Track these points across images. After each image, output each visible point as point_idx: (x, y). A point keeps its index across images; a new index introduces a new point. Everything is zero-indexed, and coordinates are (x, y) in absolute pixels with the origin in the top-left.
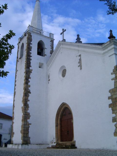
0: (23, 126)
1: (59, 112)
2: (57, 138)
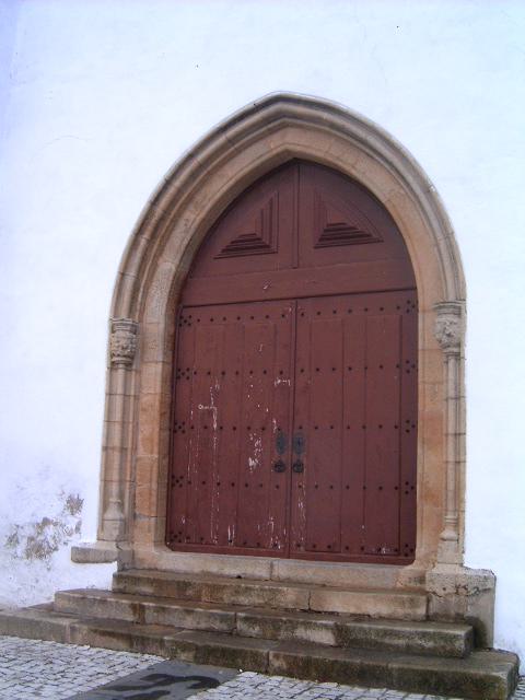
2: (121, 505)
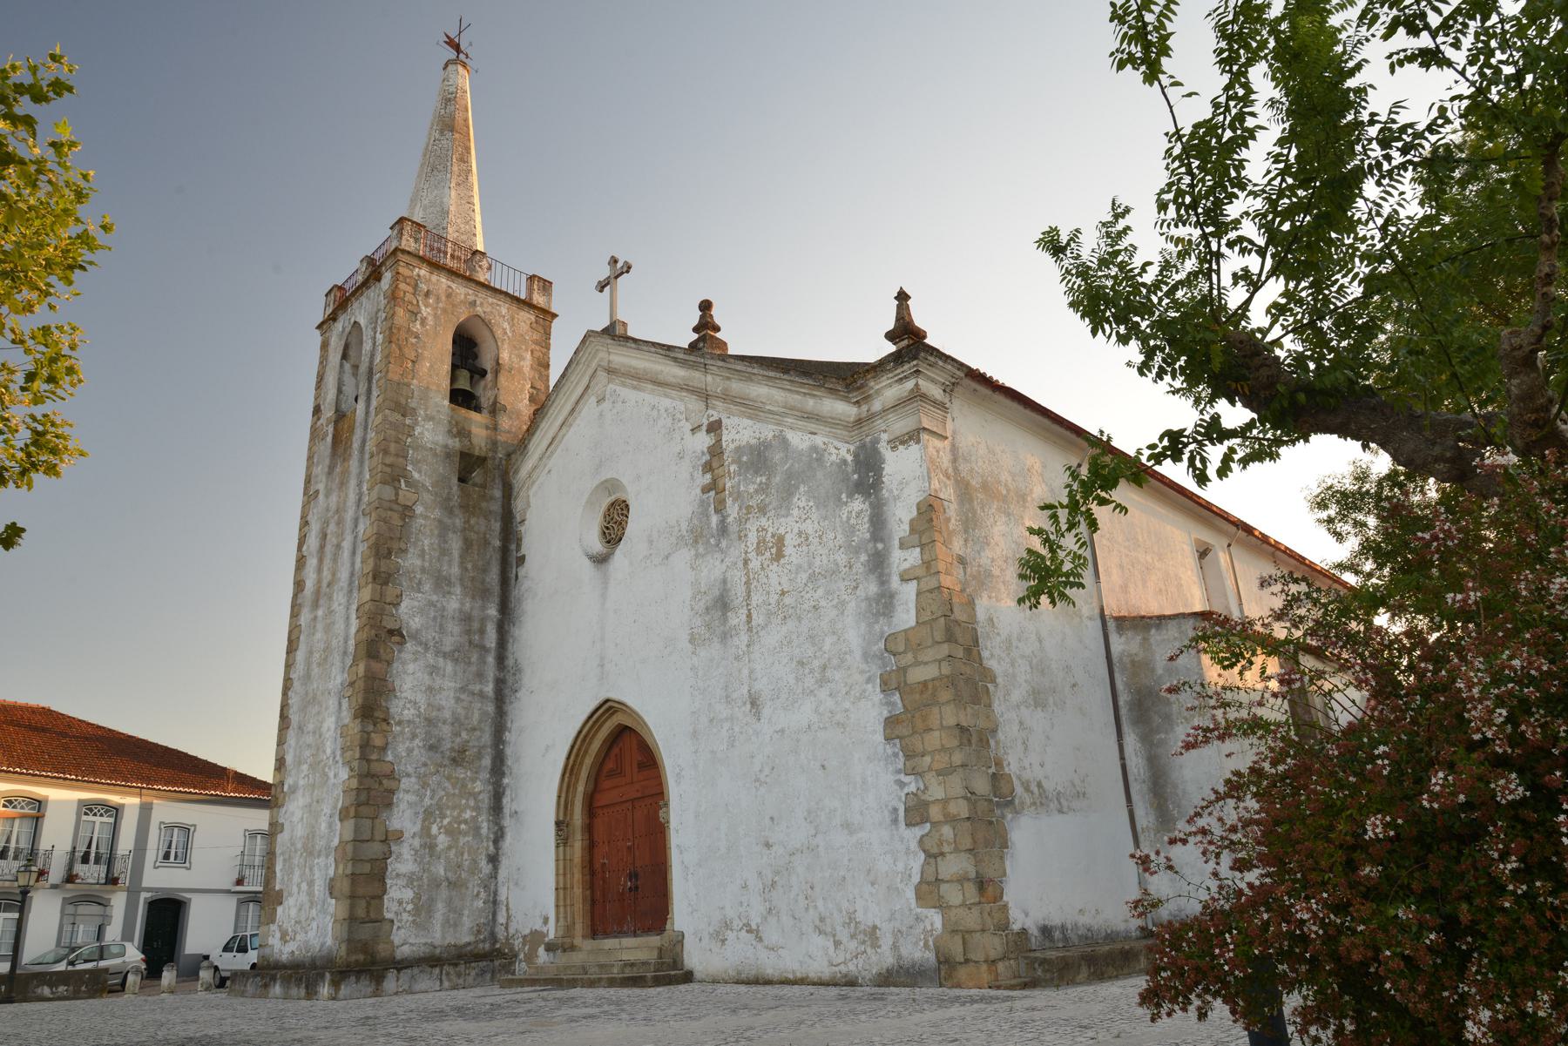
0: (349, 848)
1: (577, 755)
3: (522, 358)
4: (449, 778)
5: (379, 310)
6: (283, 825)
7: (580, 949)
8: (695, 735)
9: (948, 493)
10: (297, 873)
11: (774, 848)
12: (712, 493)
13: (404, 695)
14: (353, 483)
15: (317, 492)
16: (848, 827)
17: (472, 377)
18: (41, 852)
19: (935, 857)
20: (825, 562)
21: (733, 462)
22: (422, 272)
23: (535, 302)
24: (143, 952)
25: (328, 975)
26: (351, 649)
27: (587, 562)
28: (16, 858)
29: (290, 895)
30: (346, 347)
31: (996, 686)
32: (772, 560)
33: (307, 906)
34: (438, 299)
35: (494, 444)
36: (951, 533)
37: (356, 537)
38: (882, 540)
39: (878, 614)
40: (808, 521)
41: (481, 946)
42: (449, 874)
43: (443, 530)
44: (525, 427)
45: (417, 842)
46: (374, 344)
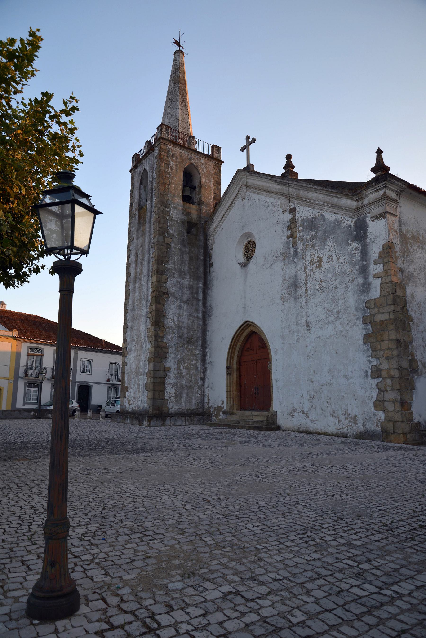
0: (152, 373)
1: (235, 342)
3: (210, 181)
4: (186, 349)
5: (154, 164)
6: (127, 363)
7: (236, 414)
8: (283, 336)
9: (396, 240)
10: (133, 381)
11: (315, 383)
12: (291, 239)
13: (170, 317)
14: (147, 235)
15: (133, 238)
16: (346, 377)
17: (190, 190)
18: (43, 368)
19: (383, 391)
20: (340, 269)
21: (300, 226)
22: (170, 147)
23: (214, 157)
24: (78, 403)
25: (147, 417)
26: (150, 299)
27: (238, 266)
28: (35, 369)
29: (131, 388)
30: (142, 179)
31: (413, 323)
32: (317, 267)
33: (137, 392)
34: (177, 158)
35: (200, 217)
36: (397, 258)
37: (149, 256)
38: (366, 260)
39: (363, 292)
40: (333, 252)
41: (199, 410)
42: (187, 384)
43: (182, 253)
44: (212, 210)
45: (175, 372)
46: (153, 178)
